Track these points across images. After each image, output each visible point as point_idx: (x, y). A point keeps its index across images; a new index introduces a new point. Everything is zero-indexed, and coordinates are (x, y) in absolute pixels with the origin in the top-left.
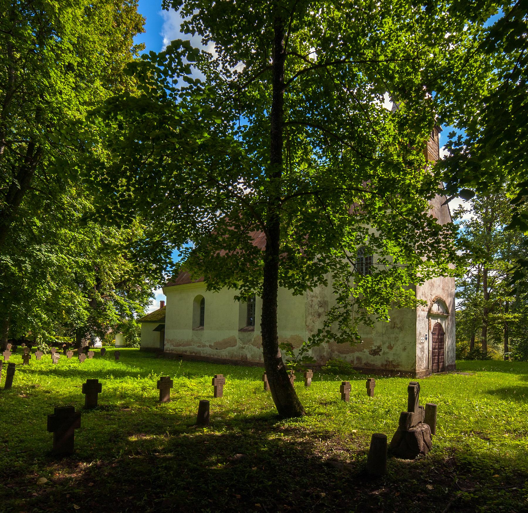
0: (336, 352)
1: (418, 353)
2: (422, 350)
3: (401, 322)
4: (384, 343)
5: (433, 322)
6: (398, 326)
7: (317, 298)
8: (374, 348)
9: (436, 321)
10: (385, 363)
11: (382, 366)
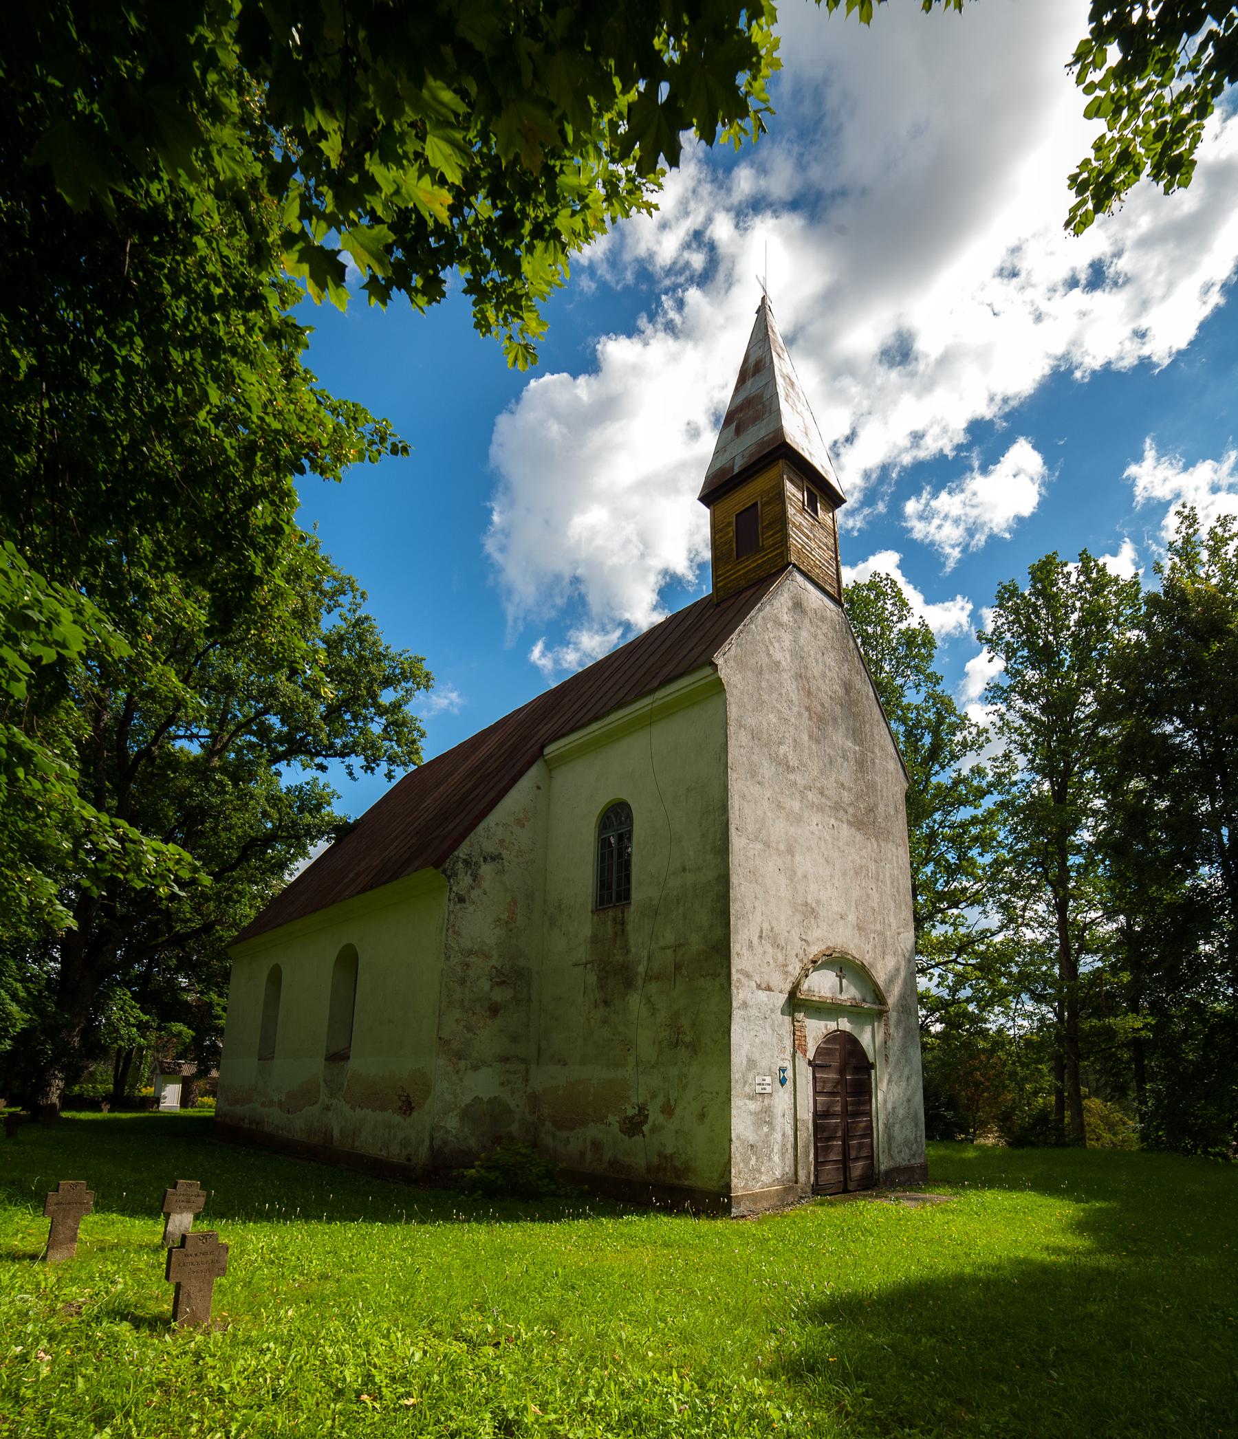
0: (548, 1125)
1: (742, 1125)
2: (765, 1117)
3: (693, 1025)
4: (654, 1096)
5: (816, 1030)
6: (688, 1039)
7: (487, 956)
8: (631, 1112)
9: (832, 1026)
10: (655, 1160)
11: (648, 1170)
